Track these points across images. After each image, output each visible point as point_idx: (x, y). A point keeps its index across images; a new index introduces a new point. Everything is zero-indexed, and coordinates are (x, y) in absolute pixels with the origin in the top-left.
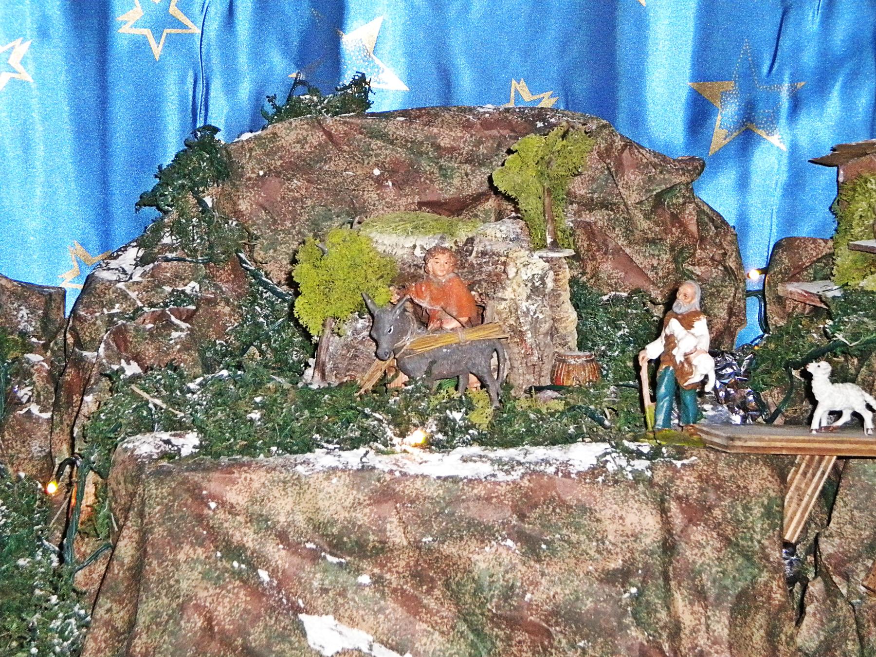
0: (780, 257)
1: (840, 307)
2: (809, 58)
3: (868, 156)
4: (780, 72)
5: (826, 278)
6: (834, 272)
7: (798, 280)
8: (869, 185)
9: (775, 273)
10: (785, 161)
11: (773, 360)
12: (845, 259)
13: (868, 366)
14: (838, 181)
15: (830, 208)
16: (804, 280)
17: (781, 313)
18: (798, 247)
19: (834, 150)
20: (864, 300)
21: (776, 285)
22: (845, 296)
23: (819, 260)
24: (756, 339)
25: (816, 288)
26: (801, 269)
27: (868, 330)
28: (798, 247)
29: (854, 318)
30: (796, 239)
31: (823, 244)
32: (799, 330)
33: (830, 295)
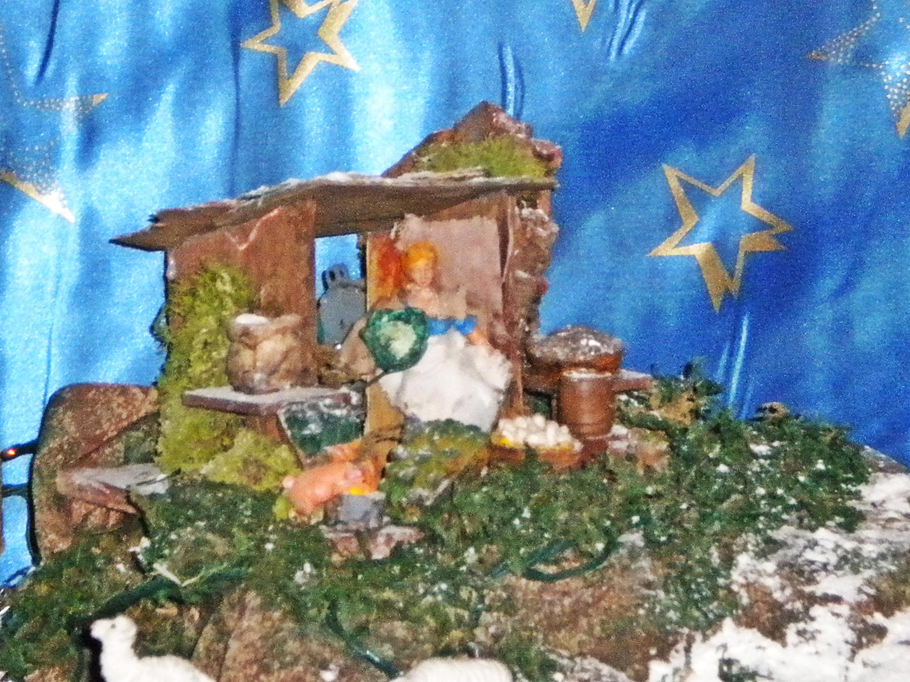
0: (61, 422)
1: (163, 512)
2: (112, 48)
3: (218, 232)
4: (60, 76)
5: (147, 458)
6: (160, 448)
7: (94, 465)
8: (219, 284)
9: (50, 452)
10: (73, 244)
11: (45, 616)
12: (177, 424)
13: (216, 623)
14: (165, 278)
15: (152, 329)
16: (107, 464)
17: (63, 527)
18: (95, 401)
19: (155, 219)
20: (207, 499)
21: (53, 475)
22: (173, 492)
23: (134, 426)
24: (13, 577)
25: (122, 479)
26: (100, 443)
27: (215, 556)
28: (95, 401)
29: (187, 534)
30: (90, 387)
31: (140, 396)
32: (91, 559)
33: (147, 490)
